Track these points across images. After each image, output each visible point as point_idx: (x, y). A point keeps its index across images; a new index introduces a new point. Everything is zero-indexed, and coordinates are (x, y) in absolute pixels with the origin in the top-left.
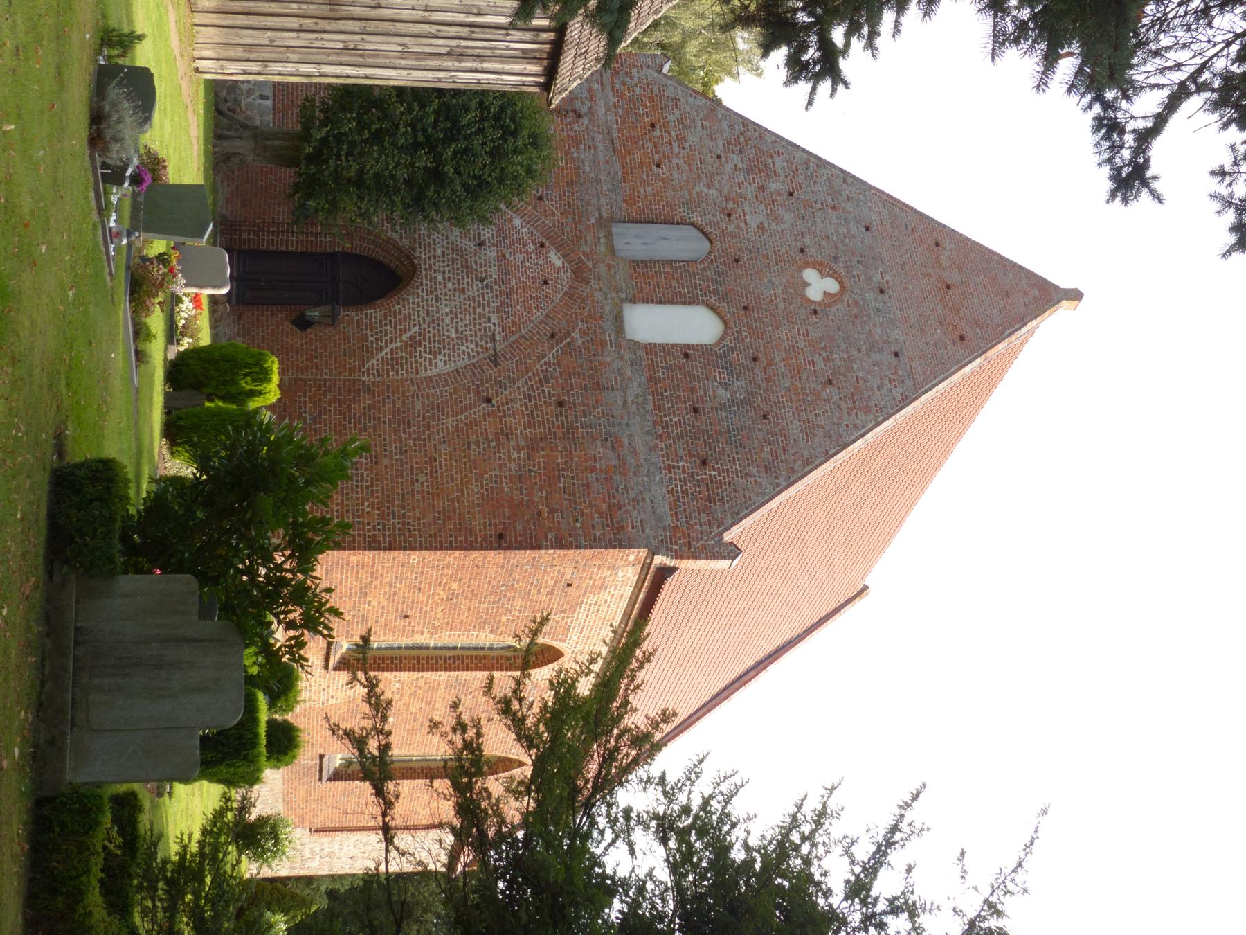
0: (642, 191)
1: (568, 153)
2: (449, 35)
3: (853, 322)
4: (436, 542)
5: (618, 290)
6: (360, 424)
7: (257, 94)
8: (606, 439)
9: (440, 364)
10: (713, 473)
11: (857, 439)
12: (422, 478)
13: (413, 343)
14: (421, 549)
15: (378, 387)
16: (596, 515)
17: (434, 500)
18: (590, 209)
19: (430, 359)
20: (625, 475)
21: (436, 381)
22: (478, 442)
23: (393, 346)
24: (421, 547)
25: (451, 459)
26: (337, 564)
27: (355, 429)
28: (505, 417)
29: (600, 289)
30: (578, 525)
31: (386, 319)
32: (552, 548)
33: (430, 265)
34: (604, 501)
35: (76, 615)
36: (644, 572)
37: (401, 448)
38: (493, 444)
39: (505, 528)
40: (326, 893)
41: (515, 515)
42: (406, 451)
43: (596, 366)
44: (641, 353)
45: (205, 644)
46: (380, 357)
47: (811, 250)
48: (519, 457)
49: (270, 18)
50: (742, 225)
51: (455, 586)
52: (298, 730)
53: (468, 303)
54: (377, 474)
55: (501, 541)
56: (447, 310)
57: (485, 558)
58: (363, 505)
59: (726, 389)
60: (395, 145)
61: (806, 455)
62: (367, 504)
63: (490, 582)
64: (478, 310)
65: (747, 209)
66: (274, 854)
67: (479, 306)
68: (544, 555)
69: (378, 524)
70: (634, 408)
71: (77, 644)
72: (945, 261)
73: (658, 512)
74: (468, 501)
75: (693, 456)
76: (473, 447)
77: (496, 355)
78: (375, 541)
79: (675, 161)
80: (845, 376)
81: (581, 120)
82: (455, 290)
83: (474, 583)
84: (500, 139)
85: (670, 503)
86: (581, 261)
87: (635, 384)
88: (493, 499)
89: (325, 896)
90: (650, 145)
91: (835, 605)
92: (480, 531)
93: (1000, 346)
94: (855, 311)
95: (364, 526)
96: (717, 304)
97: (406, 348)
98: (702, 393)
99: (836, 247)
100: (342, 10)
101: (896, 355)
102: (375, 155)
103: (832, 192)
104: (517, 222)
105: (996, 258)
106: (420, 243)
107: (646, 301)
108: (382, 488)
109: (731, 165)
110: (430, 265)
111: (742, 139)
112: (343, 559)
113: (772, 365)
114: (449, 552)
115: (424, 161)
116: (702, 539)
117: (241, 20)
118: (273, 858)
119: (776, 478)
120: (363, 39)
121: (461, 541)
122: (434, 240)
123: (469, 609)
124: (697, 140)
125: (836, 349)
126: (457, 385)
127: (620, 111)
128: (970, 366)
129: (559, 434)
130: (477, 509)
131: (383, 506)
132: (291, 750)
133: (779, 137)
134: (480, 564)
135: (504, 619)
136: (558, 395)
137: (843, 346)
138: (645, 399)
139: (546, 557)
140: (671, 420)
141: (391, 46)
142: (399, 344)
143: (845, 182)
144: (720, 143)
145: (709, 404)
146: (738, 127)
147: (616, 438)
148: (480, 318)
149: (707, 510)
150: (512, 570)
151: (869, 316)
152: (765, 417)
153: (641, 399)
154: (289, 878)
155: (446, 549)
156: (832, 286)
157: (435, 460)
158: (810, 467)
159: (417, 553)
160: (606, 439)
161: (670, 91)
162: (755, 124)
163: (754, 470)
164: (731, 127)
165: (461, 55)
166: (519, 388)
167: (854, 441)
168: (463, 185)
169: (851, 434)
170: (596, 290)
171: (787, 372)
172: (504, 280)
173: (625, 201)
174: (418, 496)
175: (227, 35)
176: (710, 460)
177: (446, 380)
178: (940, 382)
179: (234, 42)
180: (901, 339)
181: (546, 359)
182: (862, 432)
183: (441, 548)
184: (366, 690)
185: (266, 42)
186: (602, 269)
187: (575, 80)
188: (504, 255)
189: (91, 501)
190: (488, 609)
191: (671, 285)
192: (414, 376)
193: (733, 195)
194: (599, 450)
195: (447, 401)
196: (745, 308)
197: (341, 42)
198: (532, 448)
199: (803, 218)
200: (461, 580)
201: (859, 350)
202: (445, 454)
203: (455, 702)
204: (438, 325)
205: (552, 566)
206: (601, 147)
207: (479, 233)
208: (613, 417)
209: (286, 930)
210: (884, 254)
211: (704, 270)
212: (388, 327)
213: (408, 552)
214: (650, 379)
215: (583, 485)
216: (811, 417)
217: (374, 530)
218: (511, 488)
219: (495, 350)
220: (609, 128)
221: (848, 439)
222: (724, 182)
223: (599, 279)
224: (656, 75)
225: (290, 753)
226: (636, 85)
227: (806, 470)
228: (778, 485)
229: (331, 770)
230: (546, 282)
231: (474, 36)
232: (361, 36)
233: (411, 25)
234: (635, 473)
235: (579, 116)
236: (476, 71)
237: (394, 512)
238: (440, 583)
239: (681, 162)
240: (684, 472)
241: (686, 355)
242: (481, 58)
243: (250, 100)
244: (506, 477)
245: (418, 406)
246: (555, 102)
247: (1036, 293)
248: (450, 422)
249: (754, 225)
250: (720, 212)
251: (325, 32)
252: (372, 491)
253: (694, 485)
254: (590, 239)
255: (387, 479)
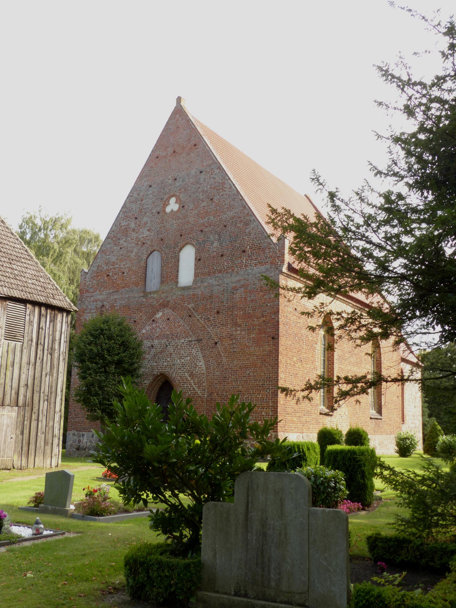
0: (133, 280)
1: (117, 310)
2: (42, 354)
3: (188, 191)
4: (275, 366)
5: (172, 289)
6: (224, 398)
7: (91, 439)
8: (233, 293)
9: (201, 364)
10: (248, 247)
11: (235, 187)
12: (248, 372)
13: (192, 375)
14: (278, 373)
15: (209, 390)
16: (265, 297)
17: (257, 367)
18: (139, 301)
19: (199, 368)
20: (248, 285)
21: (207, 365)
22: (233, 348)
23: (192, 384)
24: (277, 373)
25: (240, 360)
26: (284, 409)
27: (227, 400)
28: (223, 336)
29: (172, 296)
30: (269, 305)
31: (182, 387)
32: (279, 316)
33: (160, 368)
34: (259, 294)
35: (226, 593)
36: (290, 277)
37: (235, 381)
38: (234, 341)
39: (270, 336)
40: (429, 418)
41: (264, 332)
42: (236, 379)
43: (203, 298)
44: (198, 279)
45: (250, 500)
46: (197, 389)
47: (158, 209)
48: (240, 330)
49: (31, 434)
50: (148, 238)
51: (295, 359)
52: (350, 430)
53: (176, 352)
54: (246, 392)
55: (275, 338)
56: (178, 360)
57: (282, 345)
58: (259, 398)
59: (214, 243)
60: (105, 381)
61: (241, 208)
62: (258, 396)
63: (294, 344)
64: (179, 347)
65: (141, 236)
66: (413, 440)
67: (177, 347)
68: (282, 319)
69: (267, 391)
70: (220, 281)
71: (246, 596)
72: (164, 154)
73: (264, 271)
74: (258, 352)
75: (241, 256)
76: (235, 350)
77: (197, 340)
78: (274, 393)
79: (122, 266)
80: (209, 193)
81: (105, 305)
82: (170, 357)
83: (294, 350)
84: (104, 337)
85: (261, 266)
86: (160, 304)
87: (210, 281)
88: (257, 342)
89: (431, 419)
90: (116, 277)
91: (312, 207)
92: (271, 347)
93: (199, 129)
94: (183, 190)
95: (267, 398)
96: (179, 247)
97: (193, 378)
98: (215, 253)
99: (158, 199)
100: (28, 401)
101: (201, 172)
102: (108, 389)
103: (136, 201)
104: (144, 331)
105: (163, 133)
106: (151, 372)
107: (177, 277)
108: (252, 389)
109: (124, 243)
110: (160, 368)
111: (114, 239)
112: (282, 407)
113: (204, 224)
114: (279, 361)
115: (112, 368)
116: (276, 252)
117: (32, 447)
118: (414, 440)
119: (251, 221)
120: (43, 392)
121: (275, 355)
122: (150, 366)
123: (306, 353)
124: (114, 257)
125: (198, 197)
126: (209, 357)
127: (102, 289)
128: (206, 141)
129: (230, 313)
130: (261, 348)
131: (259, 389)
132: (360, 433)
133: (114, 224)
134: (285, 347)
135: (311, 338)
136: (215, 313)
137: (197, 195)
138: (217, 277)
139: (283, 318)
140: (226, 266)
141: (47, 380)
142: (192, 381)
143: (132, 196)
144: (115, 248)
145: (220, 250)
146: (109, 241)
147: (233, 289)
148: (182, 347)
149: (264, 250)
150: (288, 334)
151: (185, 184)
152: (225, 226)
153: (217, 278)
154: (423, 433)
155: (278, 362)
156: (173, 200)
157: (240, 366)
158: (247, 206)
159: (279, 374)
160: (233, 293)
161: (95, 269)
162: (108, 234)
163: (248, 230)
164: (109, 244)
165: (52, 349)
166: (211, 330)
167: (236, 188)
168: (124, 352)
169: (233, 190)
170: (172, 298)
171: (207, 218)
172: (167, 337)
173: (137, 286)
174: (256, 374)
175: (39, 453)
176: (243, 249)
177: (207, 361)
178: (213, 153)
179: (43, 450)
180: (195, 170)
181: (200, 319)
182: (232, 185)
183: (277, 364)
184: (313, 390)
185: (43, 435)
186: (163, 295)
187: (65, 300)
188: (157, 337)
189: (149, 577)
190: (306, 345)
191: (171, 267)
192: (205, 375)
193: (136, 242)
194: (237, 296)
195: (216, 361)
196: (181, 236)
197: (44, 402)
198: (236, 324)
199: (145, 213)
200: (293, 356)
201: (199, 188)
202: (238, 362)
203: (310, 329)
204: (184, 364)
205: (287, 316)
206: (115, 297)
207: (148, 347)
208: (224, 290)
209: (446, 435)
210: (161, 179)
211: (165, 253)
212: (185, 386)
213: (279, 378)
214: (209, 275)
215: (252, 303)
216: (226, 207)
217: (269, 393)
218: (253, 334)
219: (195, 341)
220: (108, 293)
221: (235, 191)
222: (130, 246)
223: (167, 297)
224: (88, 275)
225: (362, 433)
226: (92, 283)
227: (248, 208)
228: (254, 220)
229: (377, 414)
230: (168, 319)
231: (42, 343)
232: (41, 393)
233: (36, 371)
234: (248, 281)
235: (103, 306)
236: (60, 343)
237: (262, 384)
238: (294, 365)
239: (122, 264)
240: (248, 260)
241: (200, 260)
242: (53, 341)
243: (93, 442)
244: (248, 336)
245: (218, 373)
246: (75, 308)
247: (178, 116)
248: (224, 360)
249: (148, 233)
250: (143, 247)
251: (39, 409)
252: (253, 393)
253: (253, 255)
254: (151, 301)
255: (248, 387)
